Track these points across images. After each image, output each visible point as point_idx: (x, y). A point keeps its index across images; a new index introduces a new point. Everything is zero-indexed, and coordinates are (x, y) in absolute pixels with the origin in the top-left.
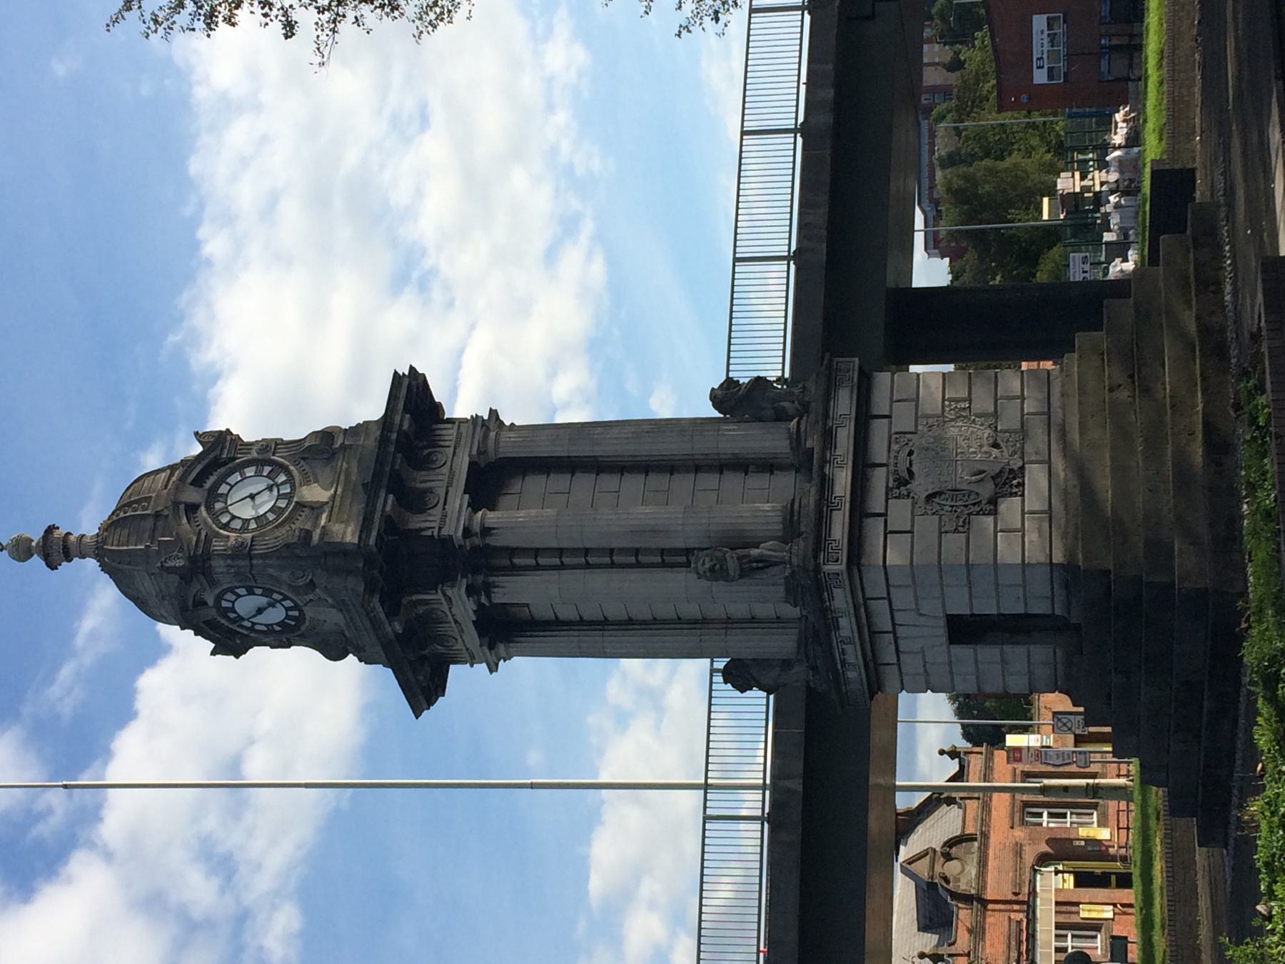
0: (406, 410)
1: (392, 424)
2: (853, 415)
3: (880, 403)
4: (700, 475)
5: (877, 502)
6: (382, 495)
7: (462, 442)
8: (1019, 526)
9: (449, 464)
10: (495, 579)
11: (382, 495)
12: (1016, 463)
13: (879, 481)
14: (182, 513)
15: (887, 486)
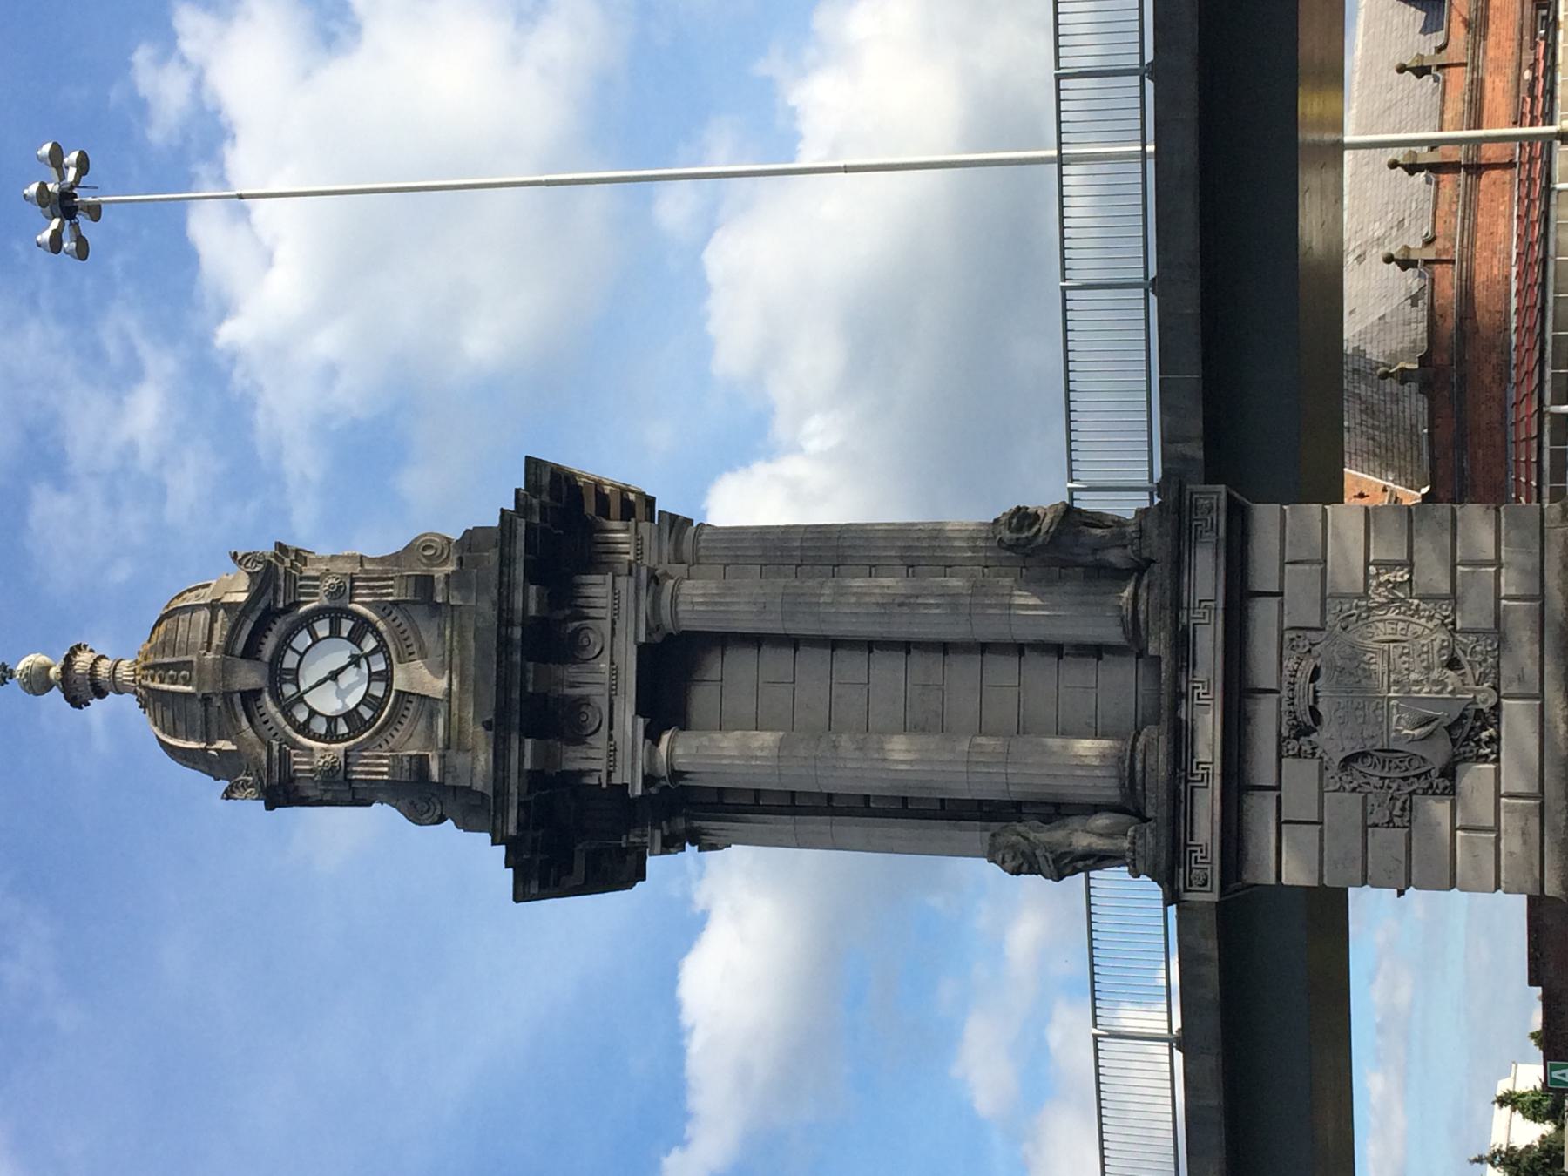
0: (530, 578)
1: (511, 610)
2: (1221, 604)
3: (1264, 574)
4: (988, 656)
5: (1263, 767)
6: (515, 744)
7: (623, 605)
9: (607, 652)
10: (704, 824)
11: (515, 744)
12: (1486, 701)
13: (1266, 719)
14: (239, 709)
15: (1279, 734)
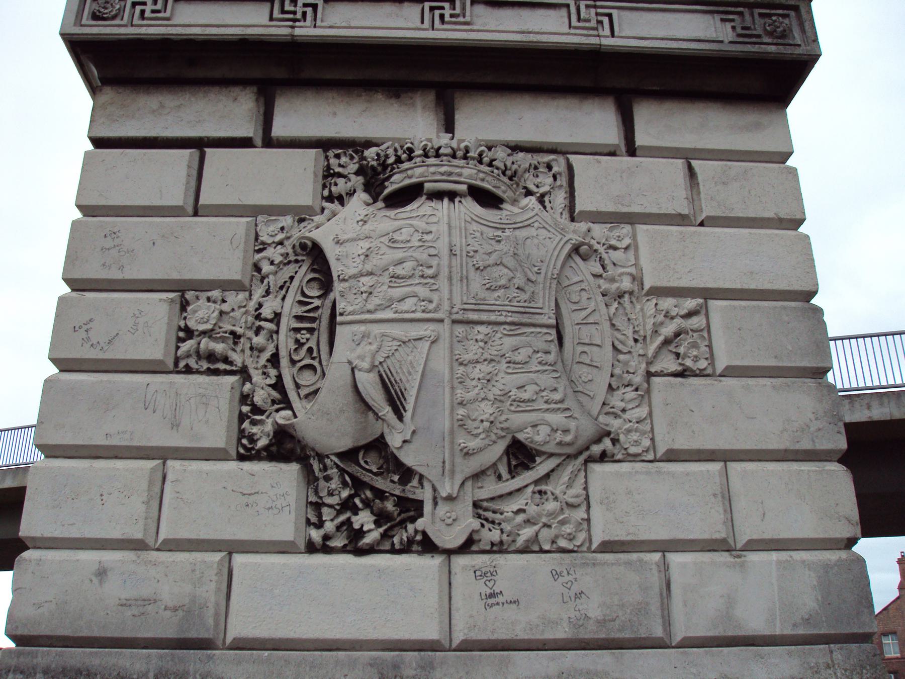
5: (297, 116)
8: (216, 557)
12: (447, 524)
